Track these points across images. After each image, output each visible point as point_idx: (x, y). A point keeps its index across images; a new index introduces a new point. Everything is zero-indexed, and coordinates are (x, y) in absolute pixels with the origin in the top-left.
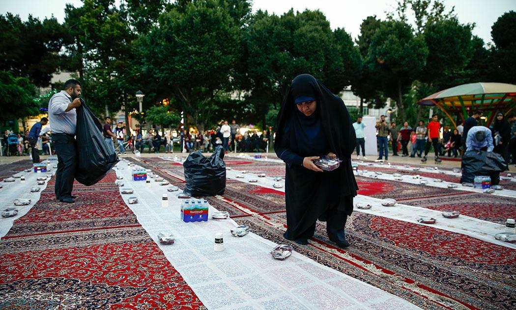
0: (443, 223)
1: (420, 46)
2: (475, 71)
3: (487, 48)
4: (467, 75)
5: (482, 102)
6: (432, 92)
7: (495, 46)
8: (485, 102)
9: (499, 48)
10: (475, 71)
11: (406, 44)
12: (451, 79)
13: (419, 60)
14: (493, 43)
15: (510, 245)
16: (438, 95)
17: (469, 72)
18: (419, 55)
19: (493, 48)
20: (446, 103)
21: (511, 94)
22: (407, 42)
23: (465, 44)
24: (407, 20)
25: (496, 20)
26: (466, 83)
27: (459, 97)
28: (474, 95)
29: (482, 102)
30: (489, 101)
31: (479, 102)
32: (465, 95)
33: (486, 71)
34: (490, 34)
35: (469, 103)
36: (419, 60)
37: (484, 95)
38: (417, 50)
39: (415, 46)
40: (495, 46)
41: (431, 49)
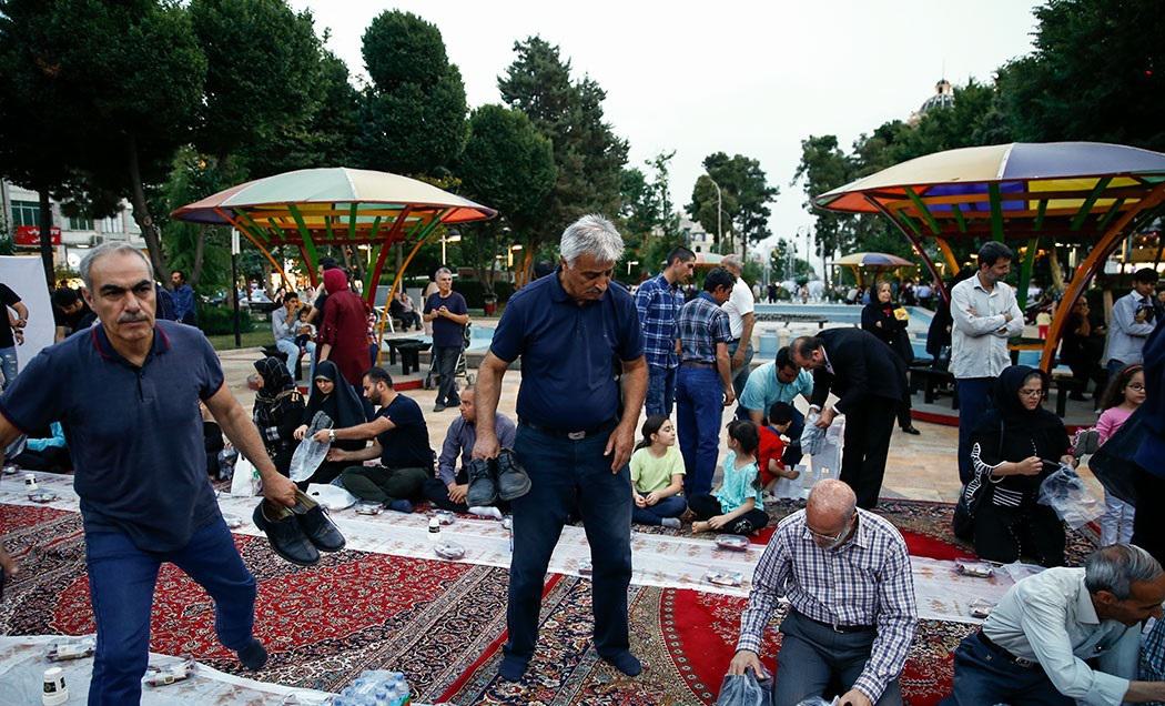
0: (852, 314)
1: (178, 41)
2: (335, 137)
3: (359, 87)
4: (319, 147)
5: (353, 219)
6: (230, 182)
7: (373, 85)
8: (360, 220)
9: (382, 92)
10: (335, 137)
11: (132, 27)
12: (281, 152)
13: (176, 83)
14: (368, 78)
15: (1078, 185)
16: (228, 196)
17: (320, 137)
18: (175, 68)
19: (368, 88)
20: (307, 220)
21: (979, 187)
22: (136, 23)
23: (302, 62)
24: (863, 137)
25: (444, 40)
26: (316, 165)
27: (291, 205)
28: (333, 204)
29: (353, 219)
30: (371, 219)
31: (345, 220)
32: (305, 203)
33: (358, 139)
34: (361, 55)
35: (320, 221)
36: (176, 83)
37: (355, 204)
38: (169, 51)
39: (160, 37)
40: (373, 85)
41: (214, 59)
